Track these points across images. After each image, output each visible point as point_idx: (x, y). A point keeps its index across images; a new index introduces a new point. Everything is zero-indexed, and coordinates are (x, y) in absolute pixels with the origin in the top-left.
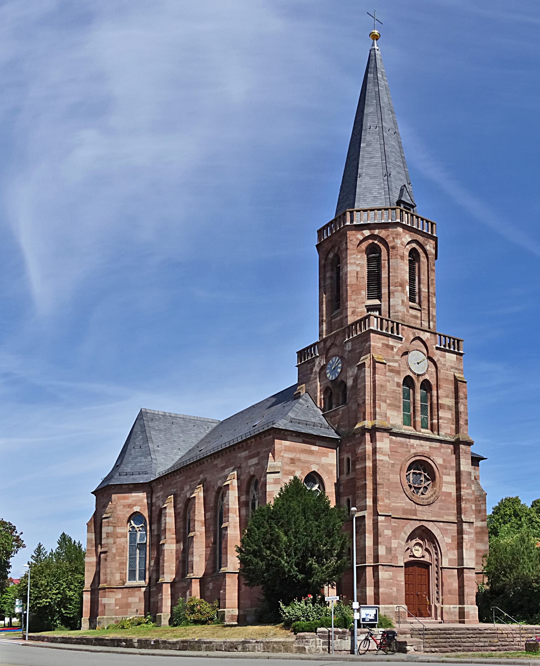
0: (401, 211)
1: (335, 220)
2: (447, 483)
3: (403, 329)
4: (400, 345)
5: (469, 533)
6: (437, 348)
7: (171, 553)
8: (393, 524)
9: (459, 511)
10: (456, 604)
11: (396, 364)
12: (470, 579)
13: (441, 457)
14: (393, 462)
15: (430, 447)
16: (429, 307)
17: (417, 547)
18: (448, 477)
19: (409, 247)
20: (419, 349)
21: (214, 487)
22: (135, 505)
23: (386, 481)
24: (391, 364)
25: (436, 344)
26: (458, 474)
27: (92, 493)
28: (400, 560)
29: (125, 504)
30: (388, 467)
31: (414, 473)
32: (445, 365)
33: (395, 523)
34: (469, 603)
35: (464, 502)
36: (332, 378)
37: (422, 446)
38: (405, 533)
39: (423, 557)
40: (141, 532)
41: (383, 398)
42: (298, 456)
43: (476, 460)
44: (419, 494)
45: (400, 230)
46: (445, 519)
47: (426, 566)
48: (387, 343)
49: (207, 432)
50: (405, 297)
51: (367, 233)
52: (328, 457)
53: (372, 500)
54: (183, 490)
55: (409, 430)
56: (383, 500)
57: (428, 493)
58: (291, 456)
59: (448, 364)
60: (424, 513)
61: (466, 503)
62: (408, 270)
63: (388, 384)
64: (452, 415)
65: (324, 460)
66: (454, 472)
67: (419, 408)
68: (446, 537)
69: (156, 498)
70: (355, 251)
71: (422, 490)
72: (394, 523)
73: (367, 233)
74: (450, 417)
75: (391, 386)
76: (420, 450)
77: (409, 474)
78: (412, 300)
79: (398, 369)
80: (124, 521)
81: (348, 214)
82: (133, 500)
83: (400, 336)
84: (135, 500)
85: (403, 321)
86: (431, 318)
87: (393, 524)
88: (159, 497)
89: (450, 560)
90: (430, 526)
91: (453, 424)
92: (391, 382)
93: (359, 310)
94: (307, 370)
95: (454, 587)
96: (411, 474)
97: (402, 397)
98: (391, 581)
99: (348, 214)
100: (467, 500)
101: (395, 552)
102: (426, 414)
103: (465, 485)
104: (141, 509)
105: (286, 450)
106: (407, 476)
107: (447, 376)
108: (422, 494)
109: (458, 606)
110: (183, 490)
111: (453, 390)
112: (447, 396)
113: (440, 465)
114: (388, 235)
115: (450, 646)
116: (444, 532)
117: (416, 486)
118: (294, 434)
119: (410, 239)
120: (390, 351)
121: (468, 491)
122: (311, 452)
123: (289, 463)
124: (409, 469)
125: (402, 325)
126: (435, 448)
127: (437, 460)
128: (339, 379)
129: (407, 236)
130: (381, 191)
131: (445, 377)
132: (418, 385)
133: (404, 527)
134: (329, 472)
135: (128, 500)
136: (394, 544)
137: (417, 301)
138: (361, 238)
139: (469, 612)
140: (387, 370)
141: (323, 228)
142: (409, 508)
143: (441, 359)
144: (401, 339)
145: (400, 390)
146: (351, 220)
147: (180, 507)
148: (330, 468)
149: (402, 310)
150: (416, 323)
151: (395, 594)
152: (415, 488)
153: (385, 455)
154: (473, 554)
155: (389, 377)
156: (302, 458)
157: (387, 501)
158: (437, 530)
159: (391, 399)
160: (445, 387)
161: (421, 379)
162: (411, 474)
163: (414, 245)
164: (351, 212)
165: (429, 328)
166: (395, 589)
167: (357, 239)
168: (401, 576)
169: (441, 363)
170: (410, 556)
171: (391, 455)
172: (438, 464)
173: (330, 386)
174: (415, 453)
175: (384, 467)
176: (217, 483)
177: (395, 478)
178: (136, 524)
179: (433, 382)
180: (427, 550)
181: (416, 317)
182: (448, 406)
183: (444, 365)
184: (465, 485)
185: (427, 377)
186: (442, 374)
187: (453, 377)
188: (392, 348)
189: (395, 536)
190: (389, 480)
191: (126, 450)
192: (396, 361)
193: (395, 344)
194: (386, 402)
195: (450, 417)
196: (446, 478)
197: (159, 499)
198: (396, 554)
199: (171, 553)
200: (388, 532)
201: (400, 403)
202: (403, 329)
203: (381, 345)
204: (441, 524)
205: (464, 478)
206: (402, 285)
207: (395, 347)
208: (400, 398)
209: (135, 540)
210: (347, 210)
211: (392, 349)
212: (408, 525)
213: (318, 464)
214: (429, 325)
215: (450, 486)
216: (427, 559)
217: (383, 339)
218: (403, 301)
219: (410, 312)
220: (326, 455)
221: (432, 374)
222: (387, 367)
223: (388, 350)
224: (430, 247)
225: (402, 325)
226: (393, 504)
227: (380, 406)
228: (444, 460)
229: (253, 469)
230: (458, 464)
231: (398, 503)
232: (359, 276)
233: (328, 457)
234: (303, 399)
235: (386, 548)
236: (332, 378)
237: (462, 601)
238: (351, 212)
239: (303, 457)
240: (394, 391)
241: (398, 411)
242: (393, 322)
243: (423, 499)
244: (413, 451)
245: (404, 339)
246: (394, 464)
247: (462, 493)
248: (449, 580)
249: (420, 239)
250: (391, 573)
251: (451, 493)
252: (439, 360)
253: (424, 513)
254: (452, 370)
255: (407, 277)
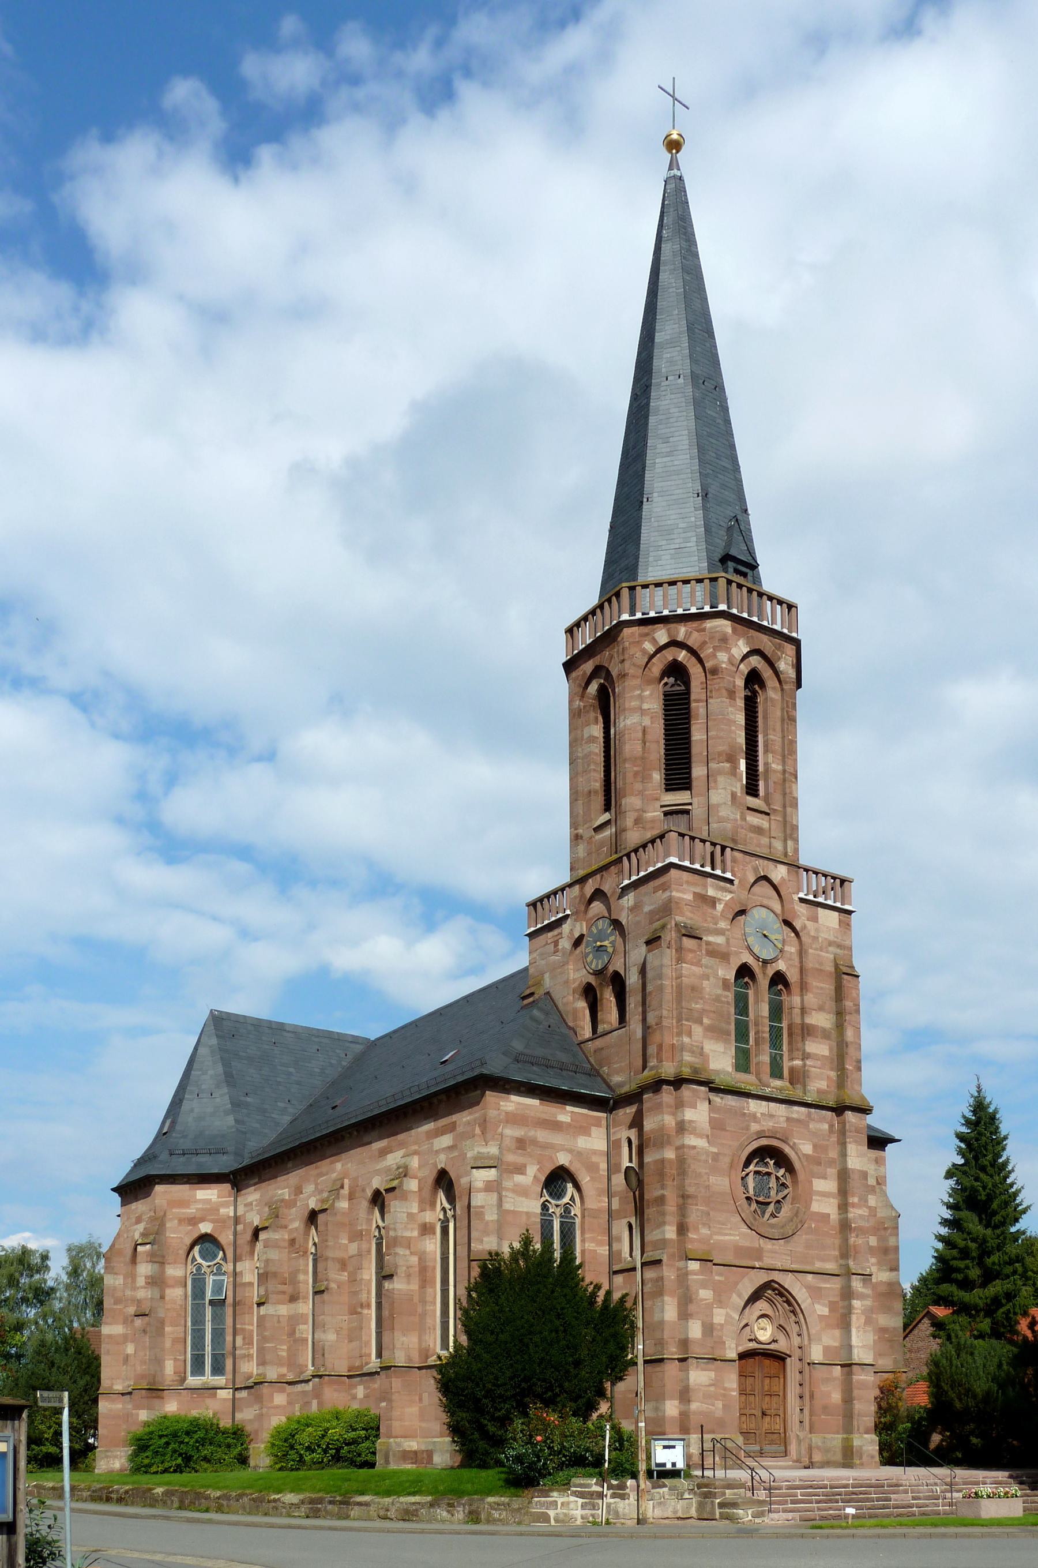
0: (729, 582)
1: (601, 606)
2: (822, 1195)
3: (734, 860)
4: (728, 897)
5: (862, 1297)
6: (802, 900)
7: (279, 1322)
8: (717, 1278)
9: (845, 1252)
10: (838, 1433)
11: (720, 940)
12: (863, 1385)
13: (806, 1137)
14: (715, 1150)
15: (788, 1119)
16: (784, 807)
17: (764, 1322)
18: (822, 1181)
19: (744, 669)
20: (765, 902)
21: (364, 1190)
22: (203, 1220)
23: (703, 1191)
24: (711, 939)
25: (799, 890)
26: (844, 1176)
27: (113, 1190)
28: (730, 1348)
29: (183, 1216)
30: (706, 1161)
31: (756, 1173)
32: (815, 938)
33: (720, 1275)
34: (862, 1430)
35: (853, 1235)
36: (597, 964)
37: (772, 1116)
38: (740, 1296)
39: (775, 1341)
40: (215, 1278)
41: (696, 1015)
42: (532, 1133)
43: (878, 1142)
44: (767, 1215)
45: (725, 626)
46: (818, 1266)
47: (780, 1358)
48: (703, 892)
49: (344, 1063)
50: (739, 785)
51: (662, 636)
52: (590, 1135)
53: (675, 1228)
54: (301, 1193)
55: (746, 1081)
56: (697, 1229)
57: (786, 1210)
58: (518, 1132)
59: (823, 935)
60: (777, 1255)
61: (857, 1236)
62: (743, 723)
63: (705, 983)
64: (831, 1050)
65: (583, 1143)
66: (832, 1172)
67: (767, 1035)
68: (819, 1303)
69: (246, 1205)
70: (638, 681)
71: (771, 1208)
72: (718, 1275)
73: (662, 636)
74: (826, 1053)
75: (710, 988)
76: (768, 1125)
77: (747, 1175)
78: (752, 789)
79: (725, 950)
80: (181, 1252)
81: (625, 593)
82: (197, 1209)
83: (728, 875)
84: (202, 1209)
85: (734, 841)
86: (788, 832)
87: (717, 1278)
88: (251, 1204)
89: (826, 1349)
90: (787, 1281)
91: (832, 1070)
92: (712, 979)
93: (649, 815)
94: (547, 944)
95: (833, 1401)
96: (751, 1176)
97: (733, 1010)
98: (712, 1389)
99: (625, 593)
100: (862, 1231)
101: (720, 1333)
102: (781, 1049)
103: (856, 1200)
104: (214, 1228)
105: (507, 1122)
106: (742, 1178)
107: (821, 964)
108: (773, 1215)
109: (840, 1436)
110: (301, 1193)
111: (833, 993)
112: (821, 1009)
113: (807, 1156)
114: (704, 643)
115: (819, 1509)
116: (816, 1293)
117: (760, 1199)
118: (522, 1089)
119: (745, 650)
120: (710, 910)
121: (860, 1212)
122: (556, 1126)
123: (513, 1147)
124: (747, 1163)
125: (732, 849)
126: (798, 1121)
127: (801, 1147)
128: (611, 969)
129: (741, 643)
130: (689, 534)
131: (817, 966)
132: (764, 982)
133: (736, 1284)
134: (592, 1168)
135: (188, 1207)
136: (719, 1317)
137: (762, 793)
138: (650, 648)
139: (861, 1447)
140: (704, 952)
141: (577, 624)
142: (747, 1244)
143: (810, 925)
144: (731, 882)
145: (730, 996)
146: (631, 609)
147: (296, 1229)
148: (595, 1159)
149: (732, 816)
150: (759, 845)
151: (719, 1413)
152: (758, 1202)
153: (700, 1136)
154: (871, 1338)
155: (706, 967)
156: (540, 1139)
157: (704, 1231)
158: (800, 1289)
159: (712, 1015)
160: (817, 987)
161: (771, 971)
162: (751, 1176)
163: (755, 661)
164: (632, 589)
165: (786, 855)
166: (719, 1404)
167: (644, 651)
168: (731, 1381)
169: (808, 934)
170: (750, 1340)
171: (712, 1135)
172: (804, 1155)
173: (594, 983)
174: (758, 1132)
175: (699, 1161)
176: (369, 1183)
177: (720, 1183)
178: (204, 1258)
179: (792, 976)
180: (781, 1327)
181: (759, 830)
182: (824, 1030)
183: (814, 937)
184: (856, 1200)
185: (781, 966)
186: (810, 957)
187: (832, 964)
188: (713, 902)
189: (720, 1302)
190: (708, 1187)
191: (181, 1101)
192: (720, 932)
193: (719, 895)
194: (701, 1023)
195: (826, 1053)
196: (820, 1185)
197: (252, 1210)
198: (721, 1337)
199: (279, 1322)
200: (705, 1294)
201: (730, 1024)
202: (734, 860)
203: (689, 897)
204: (810, 1277)
205: (855, 1183)
206: (732, 759)
207: (719, 900)
208: (729, 1014)
209: (204, 1293)
210: (624, 585)
211: (714, 906)
212: (746, 1280)
213: (570, 1151)
214: (785, 848)
215: (826, 1199)
216: (782, 1346)
217: (695, 884)
218: (734, 795)
219: (748, 818)
220: (585, 1131)
221: (790, 959)
222: (704, 946)
223: (705, 907)
224: (785, 665)
225: (732, 849)
226: (716, 1237)
227: (690, 1032)
228: (815, 1147)
229: (442, 1157)
230: (844, 1155)
231: (727, 1235)
232: (648, 737)
233: (590, 1135)
234: (541, 1009)
235: (703, 1325)
236: (597, 964)
237: (848, 1428)
238: (632, 589)
239: (542, 1135)
240: (717, 999)
241: (726, 1042)
242: (714, 844)
243: (772, 1226)
244: (755, 1127)
245: (736, 882)
246: (717, 1154)
247: (850, 1215)
248: (824, 1388)
249: (766, 643)
250: (712, 1374)
251: (829, 1215)
252: (804, 927)
253: (777, 1255)
254: (831, 949)
255: (741, 739)
